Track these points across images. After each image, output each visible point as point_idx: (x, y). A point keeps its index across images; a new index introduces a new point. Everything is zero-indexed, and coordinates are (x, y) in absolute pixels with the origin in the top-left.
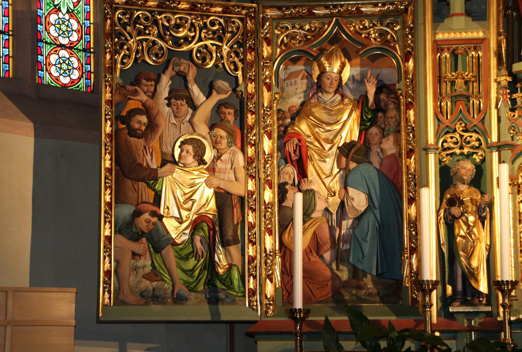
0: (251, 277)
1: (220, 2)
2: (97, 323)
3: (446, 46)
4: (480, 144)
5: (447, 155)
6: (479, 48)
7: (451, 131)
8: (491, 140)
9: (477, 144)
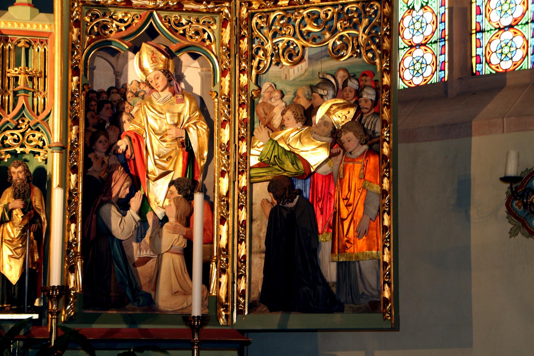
0: (386, 285)
1: (331, 3)
2: (398, 330)
3: (39, 38)
4: (44, 144)
5: (7, 152)
6: (45, 43)
7: (12, 128)
8: (53, 141)
9: (41, 144)
